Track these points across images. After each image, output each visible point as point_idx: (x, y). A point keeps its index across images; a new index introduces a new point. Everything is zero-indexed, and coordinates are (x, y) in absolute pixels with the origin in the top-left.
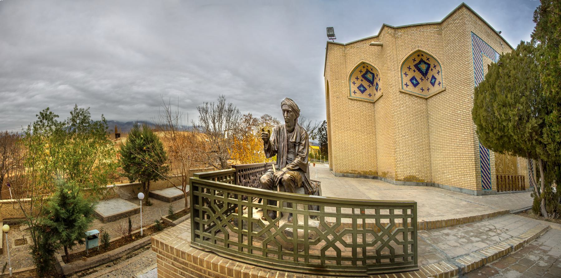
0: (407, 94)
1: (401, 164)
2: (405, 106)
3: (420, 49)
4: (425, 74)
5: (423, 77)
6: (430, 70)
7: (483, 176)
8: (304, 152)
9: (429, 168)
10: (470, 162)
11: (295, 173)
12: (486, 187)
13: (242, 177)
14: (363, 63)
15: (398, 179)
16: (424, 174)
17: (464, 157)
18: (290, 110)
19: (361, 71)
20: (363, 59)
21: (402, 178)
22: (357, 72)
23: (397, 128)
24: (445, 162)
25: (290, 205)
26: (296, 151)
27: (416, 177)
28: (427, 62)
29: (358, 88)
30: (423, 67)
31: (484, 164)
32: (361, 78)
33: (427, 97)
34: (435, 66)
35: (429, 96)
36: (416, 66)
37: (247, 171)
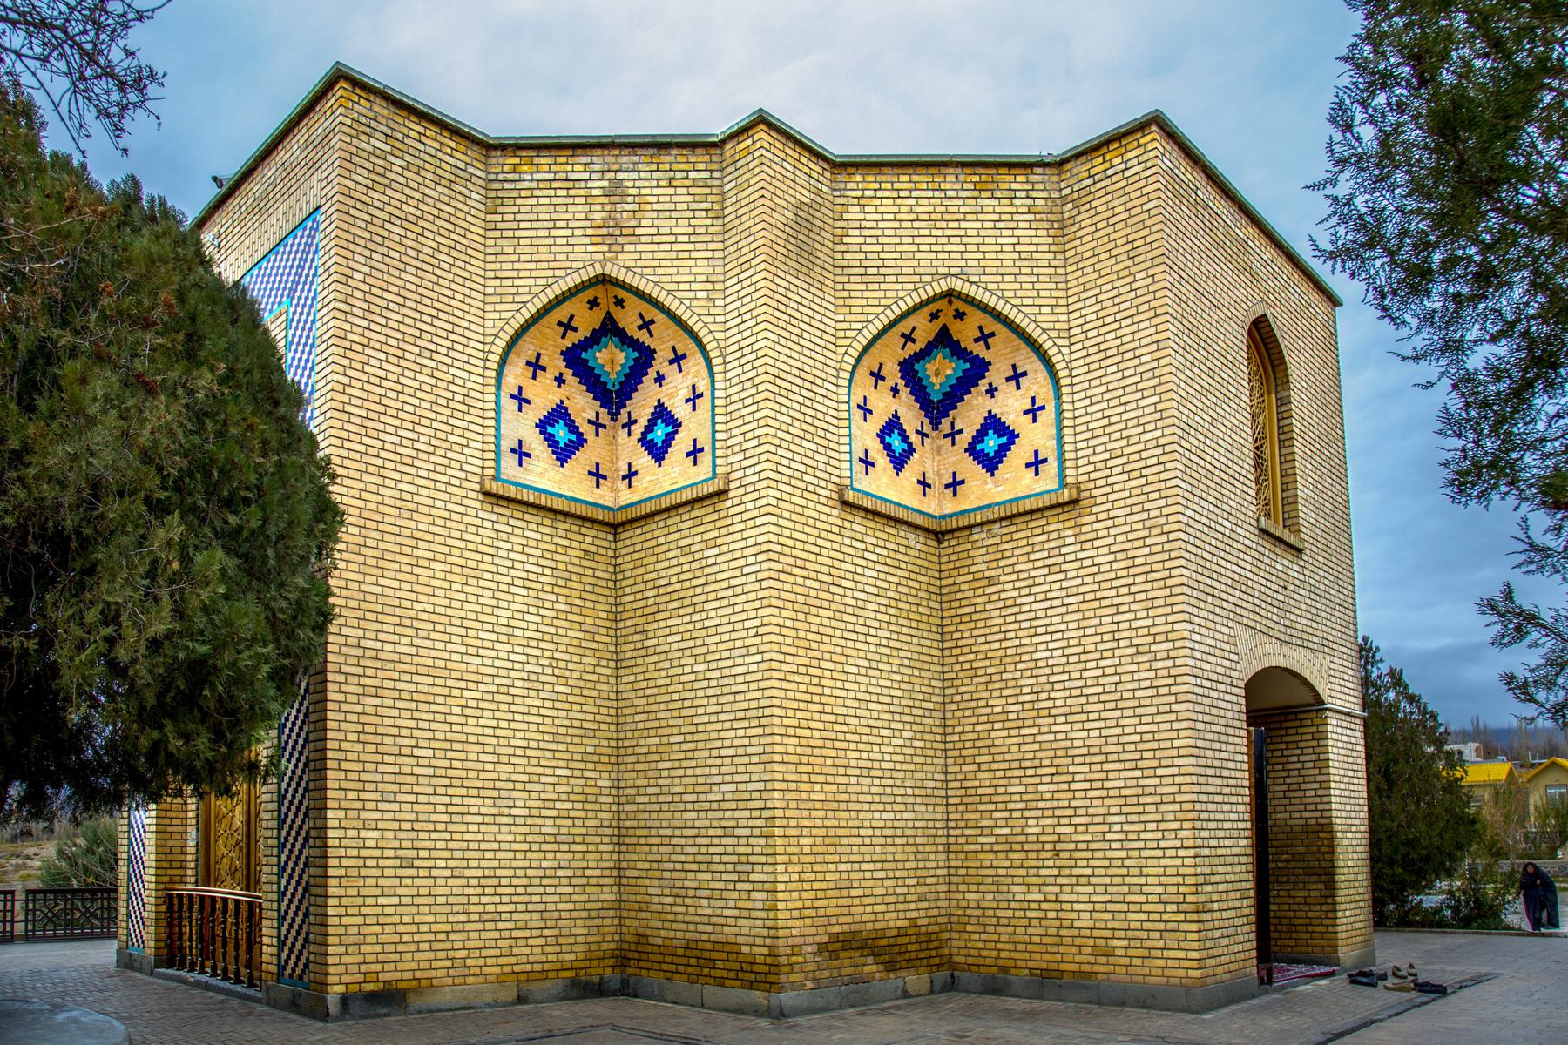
4: (613, 398)
5: (603, 412)
19: (567, 326)
28: (643, 336)
29: (542, 425)
30: (611, 360)
33: (621, 517)
36: (575, 359)
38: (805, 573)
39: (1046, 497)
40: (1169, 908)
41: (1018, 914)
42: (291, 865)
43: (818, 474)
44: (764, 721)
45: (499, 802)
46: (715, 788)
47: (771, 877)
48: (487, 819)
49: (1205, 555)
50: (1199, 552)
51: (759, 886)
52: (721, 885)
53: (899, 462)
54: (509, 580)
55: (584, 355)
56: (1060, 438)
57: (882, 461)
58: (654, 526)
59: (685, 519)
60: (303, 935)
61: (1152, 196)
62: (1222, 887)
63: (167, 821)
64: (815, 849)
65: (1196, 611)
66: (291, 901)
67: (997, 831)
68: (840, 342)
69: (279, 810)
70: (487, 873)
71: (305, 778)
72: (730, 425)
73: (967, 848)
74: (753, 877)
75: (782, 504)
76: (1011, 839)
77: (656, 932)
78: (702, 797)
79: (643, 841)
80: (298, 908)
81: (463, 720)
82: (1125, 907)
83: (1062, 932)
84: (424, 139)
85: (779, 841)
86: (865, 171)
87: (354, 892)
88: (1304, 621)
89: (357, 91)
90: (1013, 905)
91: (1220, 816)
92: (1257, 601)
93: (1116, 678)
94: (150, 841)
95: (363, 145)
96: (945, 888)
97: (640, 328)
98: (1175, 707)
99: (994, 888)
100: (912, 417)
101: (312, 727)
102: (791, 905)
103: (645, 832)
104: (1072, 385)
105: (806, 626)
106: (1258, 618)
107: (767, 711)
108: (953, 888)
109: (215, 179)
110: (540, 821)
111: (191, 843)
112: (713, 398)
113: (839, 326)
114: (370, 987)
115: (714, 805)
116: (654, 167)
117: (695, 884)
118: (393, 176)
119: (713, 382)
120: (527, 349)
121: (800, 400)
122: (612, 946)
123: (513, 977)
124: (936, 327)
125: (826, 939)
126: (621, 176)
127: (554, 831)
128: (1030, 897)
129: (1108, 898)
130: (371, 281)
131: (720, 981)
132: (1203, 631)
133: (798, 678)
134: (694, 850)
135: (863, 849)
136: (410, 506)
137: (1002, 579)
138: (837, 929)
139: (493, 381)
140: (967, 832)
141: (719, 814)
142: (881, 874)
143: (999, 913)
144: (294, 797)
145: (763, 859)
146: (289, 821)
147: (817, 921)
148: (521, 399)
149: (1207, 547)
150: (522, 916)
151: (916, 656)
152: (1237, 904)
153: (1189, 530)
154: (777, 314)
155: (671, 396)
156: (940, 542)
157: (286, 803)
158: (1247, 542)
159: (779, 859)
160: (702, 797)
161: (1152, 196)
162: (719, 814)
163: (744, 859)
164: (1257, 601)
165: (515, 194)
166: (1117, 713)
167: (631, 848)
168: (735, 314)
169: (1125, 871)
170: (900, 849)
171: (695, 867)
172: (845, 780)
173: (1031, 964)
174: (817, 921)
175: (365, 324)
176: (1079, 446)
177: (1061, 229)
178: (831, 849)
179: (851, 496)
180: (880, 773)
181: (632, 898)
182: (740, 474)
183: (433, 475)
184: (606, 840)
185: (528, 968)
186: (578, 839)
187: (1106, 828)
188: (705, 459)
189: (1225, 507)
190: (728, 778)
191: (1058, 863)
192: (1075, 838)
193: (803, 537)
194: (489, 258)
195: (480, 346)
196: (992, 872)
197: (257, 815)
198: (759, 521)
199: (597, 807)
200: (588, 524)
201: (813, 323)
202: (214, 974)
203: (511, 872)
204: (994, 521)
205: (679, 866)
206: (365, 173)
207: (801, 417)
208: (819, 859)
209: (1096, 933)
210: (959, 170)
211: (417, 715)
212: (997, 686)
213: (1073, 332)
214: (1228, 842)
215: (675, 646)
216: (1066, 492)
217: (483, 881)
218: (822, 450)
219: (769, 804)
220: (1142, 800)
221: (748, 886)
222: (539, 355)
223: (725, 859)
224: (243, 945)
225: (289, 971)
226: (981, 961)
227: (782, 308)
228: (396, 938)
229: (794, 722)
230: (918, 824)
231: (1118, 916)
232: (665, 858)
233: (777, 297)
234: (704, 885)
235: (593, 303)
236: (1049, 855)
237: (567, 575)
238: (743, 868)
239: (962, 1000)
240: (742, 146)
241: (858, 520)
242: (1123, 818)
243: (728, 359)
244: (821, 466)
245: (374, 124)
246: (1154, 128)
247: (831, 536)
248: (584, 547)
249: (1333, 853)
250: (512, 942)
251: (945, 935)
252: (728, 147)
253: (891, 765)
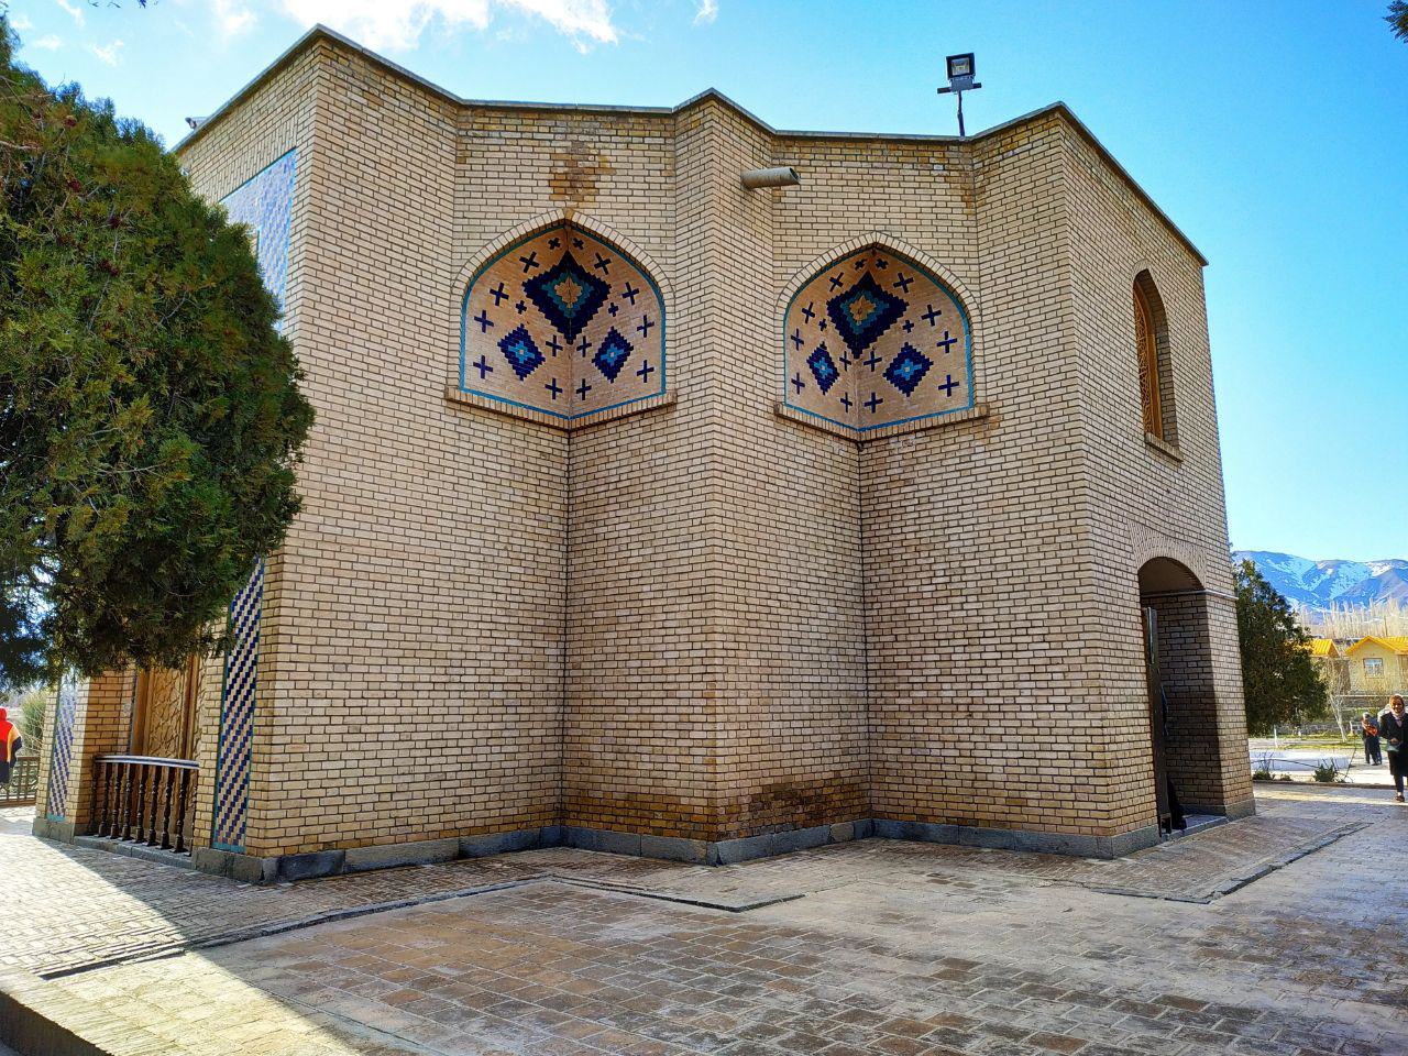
5: (560, 335)
19: (530, 262)
22: (513, 262)
28: (599, 274)
29: (504, 345)
33: (576, 424)
36: (535, 289)
38: (745, 473)
40: (1078, 764)
41: (934, 767)
42: (233, 733)
43: (756, 391)
44: (705, 598)
45: (450, 671)
46: (659, 655)
47: (711, 735)
48: (437, 687)
49: (1103, 463)
50: (1098, 460)
51: (700, 743)
52: (663, 742)
53: (825, 384)
54: (469, 475)
55: (544, 287)
56: (971, 365)
57: (812, 383)
58: (606, 432)
59: (635, 428)
60: (241, 800)
61: (1055, 170)
62: (1125, 746)
63: (101, 694)
64: (751, 709)
65: (1096, 509)
66: (230, 768)
67: (914, 694)
68: (776, 284)
69: (224, 683)
70: (434, 735)
71: (254, 652)
72: (678, 350)
73: (885, 708)
74: (693, 735)
75: (726, 416)
76: (927, 701)
77: (596, 786)
78: (646, 663)
79: (587, 702)
80: (238, 775)
81: (419, 597)
82: (1037, 763)
83: (977, 784)
84: (398, 96)
85: (719, 702)
86: (802, 143)
87: (299, 758)
88: (1185, 520)
90: (929, 759)
91: (1121, 684)
92: (1147, 503)
93: (1024, 565)
94: (81, 712)
95: (340, 97)
96: (865, 743)
97: (597, 266)
98: (1079, 590)
99: (912, 744)
100: (836, 346)
101: (265, 605)
102: (728, 760)
103: (590, 695)
104: (982, 322)
105: (745, 518)
106: (1147, 516)
107: (709, 589)
108: (874, 743)
109: (189, 120)
110: (490, 687)
111: (123, 714)
112: (664, 327)
113: (776, 270)
114: (307, 849)
115: (658, 671)
116: (614, 132)
117: (637, 741)
118: (368, 125)
119: (664, 313)
120: (492, 280)
121: (742, 330)
122: (553, 800)
123: (456, 832)
124: (862, 271)
125: (759, 790)
126: (582, 138)
127: (503, 695)
128: (945, 753)
129: (1020, 754)
130: (345, 213)
131: (659, 831)
132: (1103, 526)
133: (737, 561)
134: (637, 710)
135: (793, 709)
136: (375, 409)
137: (917, 481)
138: (770, 781)
139: (459, 305)
140: (885, 694)
141: (662, 679)
142: (809, 731)
143: (916, 766)
144: (241, 669)
145: (703, 718)
146: (233, 692)
147: (751, 775)
148: (484, 322)
149: (1104, 456)
150: (466, 775)
151: (839, 544)
152: (1138, 761)
153: (1089, 442)
154: (724, 258)
155: (623, 324)
156: (860, 450)
157: (232, 675)
158: (1136, 453)
159: (719, 718)
160: (646, 663)
161: (1055, 170)
162: (662, 679)
163: (685, 718)
164: (1147, 503)
165: (484, 148)
166: (1025, 594)
167: (575, 710)
168: (686, 284)
169: (1035, 731)
170: (825, 709)
171: (637, 726)
172: (778, 648)
173: (948, 813)
174: (751, 775)
175: (338, 250)
176: (988, 372)
177: (972, 196)
178: (765, 709)
179: (785, 411)
180: (808, 643)
181: (574, 754)
182: (688, 390)
183: (398, 383)
184: (551, 702)
185: (471, 823)
186: (524, 702)
187: (1017, 693)
188: (655, 377)
189: (1118, 424)
190: (671, 647)
191: (972, 722)
192: (987, 700)
193: (743, 444)
194: (457, 201)
195: (448, 275)
196: (909, 730)
197: (198, 686)
198: (704, 430)
200: (819, 433)
201: (754, 266)
202: (141, 839)
203: (458, 735)
204: (910, 433)
205: (622, 726)
206: (342, 121)
207: (743, 344)
208: (754, 718)
209: (1009, 786)
210: (884, 146)
211: (372, 593)
212: (912, 569)
213: (983, 279)
214: (1128, 707)
215: (623, 533)
216: (976, 410)
217: (430, 744)
218: (760, 372)
219: (710, 669)
220: (1050, 669)
221: (689, 743)
222: (502, 286)
223: (666, 718)
224: (174, 812)
225: (223, 834)
226: (900, 810)
227: (727, 253)
228: (339, 800)
229: (734, 599)
230: (841, 687)
231: (1029, 771)
232: (608, 718)
233: (723, 244)
234: (646, 742)
235: (554, 244)
236: (963, 715)
237: (524, 472)
238: (684, 725)
239: (883, 845)
240: (694, 118)
241: (790, 430)
242: (1033, 685)
243: (678, 295)
244: (759, 385)
245: (351, 80)
246: (1057, 115)
247: (767, 443)
248: (540, 448)
249: (1215, 716)
250: (456, 800)
251: (867, 786)
252: (680, 119)
253: (818, 636)
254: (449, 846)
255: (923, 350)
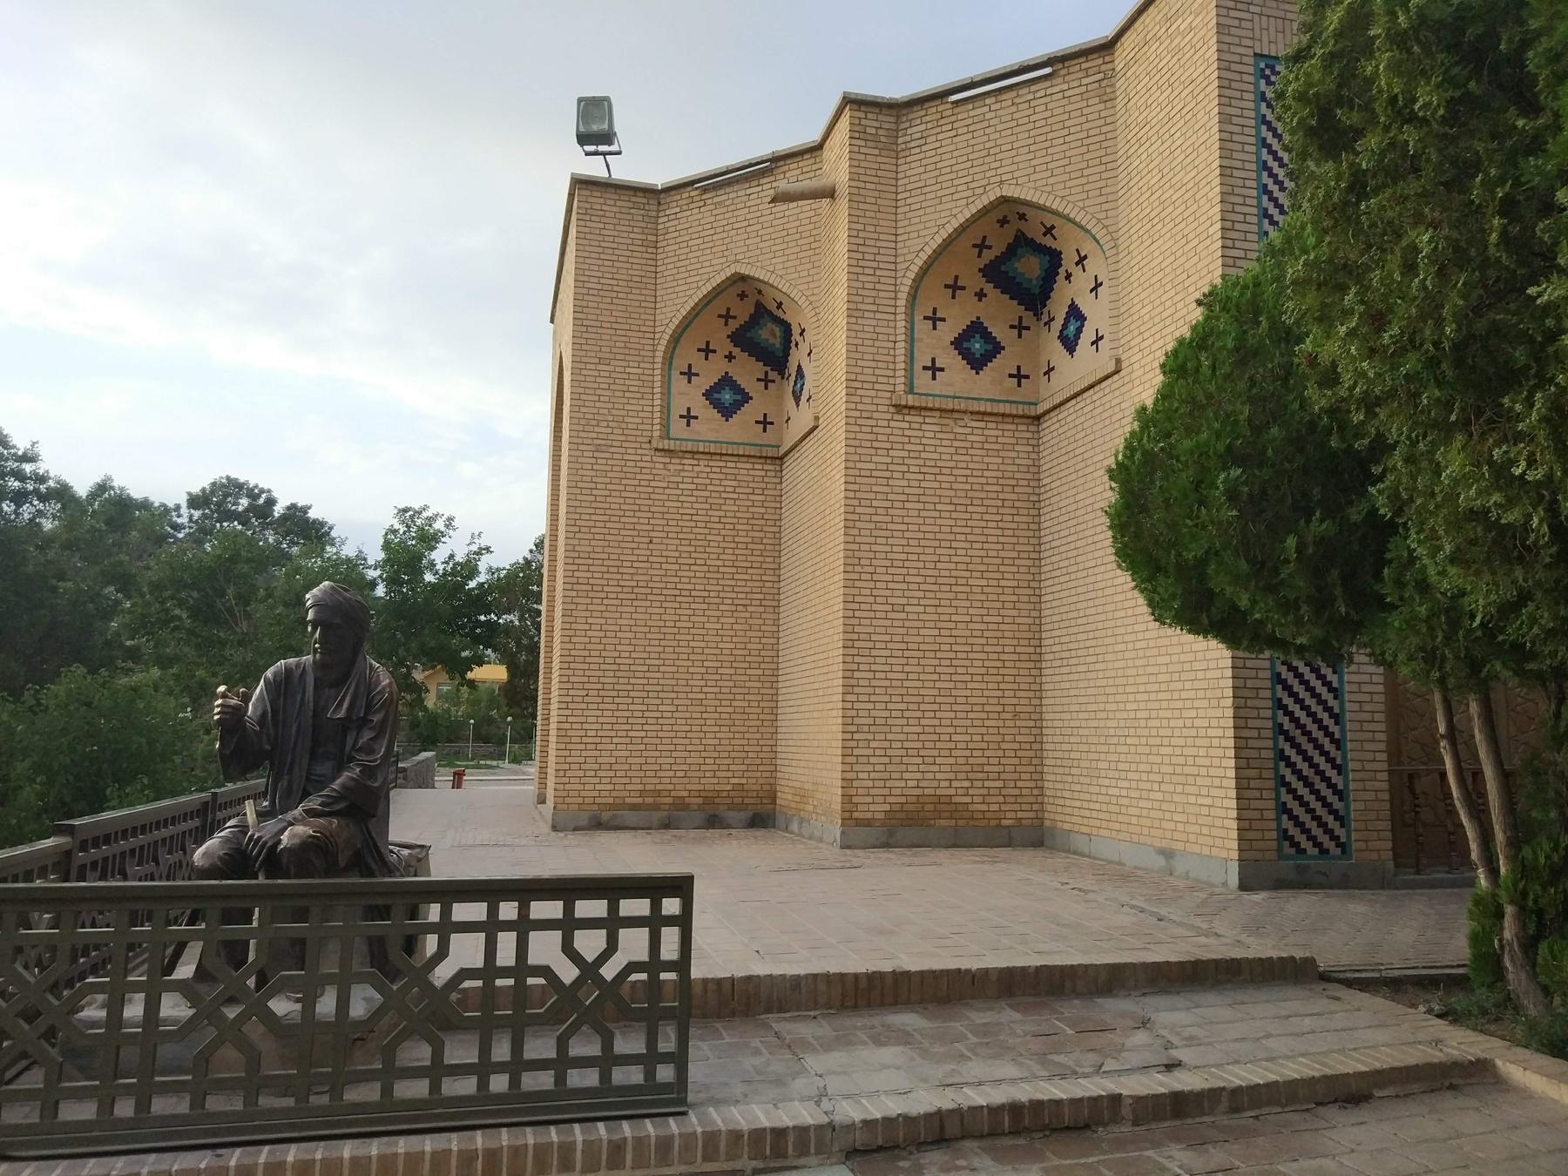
0: (931, 409)
1: (873, 744)
2: (912, 469)
3: (1009, 191)
6: (1061, 277)
7: (1289, 777)
8: (376, 747)
9: (1031, 753)
10: (1211, 713)
11: (331, 823)
12: (1305, 844)
13: (190, 835)
14: (743, 278)
15: (855, 815)
16: (999, 784)
17: (1188, 685)
18: (337, 621)
19: (727, 317)
20: (737, 261)
21: (879, 809)
23: (864, 577)
24: (1104, 715)
25: (302, 915)
26: (348, 748)
27: (956, 800)
28: (1048, 241)
29: (708, 394)
30: (1029, 267)
31: (1299, 713)
32: (723, 345)
34: (1081, 260)
35: (1046, 406)
36: (739, 338)
37: (116, 841)
39: (765, 449)
59: (1080, 403)
89: (863, 108)
148: (934, 319)
199: (920, 639)
235: (742, 296)
254: (584, 819)
255: (743, 382)
